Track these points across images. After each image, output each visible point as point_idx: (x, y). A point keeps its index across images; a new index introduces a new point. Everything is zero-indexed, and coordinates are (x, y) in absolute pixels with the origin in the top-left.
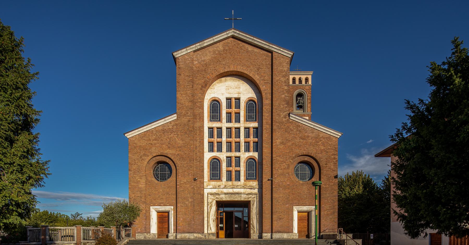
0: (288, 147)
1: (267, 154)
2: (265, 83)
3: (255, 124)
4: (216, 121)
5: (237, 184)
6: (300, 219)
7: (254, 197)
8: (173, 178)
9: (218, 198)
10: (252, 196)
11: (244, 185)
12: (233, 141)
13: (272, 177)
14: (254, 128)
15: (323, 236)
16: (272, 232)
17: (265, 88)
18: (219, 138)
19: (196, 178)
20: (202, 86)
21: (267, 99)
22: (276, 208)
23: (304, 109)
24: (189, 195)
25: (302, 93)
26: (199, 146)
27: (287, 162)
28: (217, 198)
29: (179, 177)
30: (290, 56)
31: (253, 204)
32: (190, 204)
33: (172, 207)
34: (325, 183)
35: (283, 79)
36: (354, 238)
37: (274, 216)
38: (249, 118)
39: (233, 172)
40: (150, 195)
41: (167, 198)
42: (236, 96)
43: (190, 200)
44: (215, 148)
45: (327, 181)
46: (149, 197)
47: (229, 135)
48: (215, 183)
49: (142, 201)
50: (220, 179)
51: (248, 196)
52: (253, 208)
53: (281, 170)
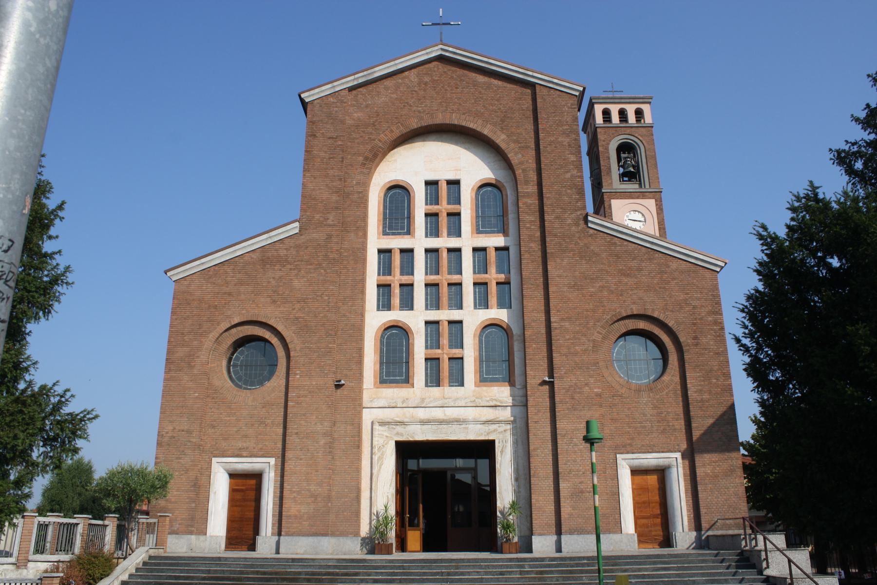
0: (591, 296)
1: (536, 315)
2: (520, 147)
3: (499, 241)
4: (399, 234)
6: (638, 491)
7: (505, 431)
8: (277, 382)
9: (402, 435)
10: (499, 427)
12: (444, 281)
13: (551, 375)
14: (497, 249)
15: (710, 538)
16: (559, 533)
17: (523, 159)
18: (408, 274)
19: (340, 381)
20: (366, 158)
21: (527, 182)
22: (568, 461)
23: (640, 181)
24: (319, 427)
25: (632, 143)
28: (398, 434)
29: (295, 379)
30: (577, 94)
31: (503, 448)
33: (272, 461)
34: (700, 388)
35: (566, 141)
36: (792, 544)
37: (563, 485)
38: (481, 228)
39: (443, 362)
40: (213, 427)
41: (260, 434)
42: (452, 177)
44: (396, 301)
45: (703, 383)
46: (211, 431)
47: (433, 267)
49: (190, 441)
50: (407, 380)
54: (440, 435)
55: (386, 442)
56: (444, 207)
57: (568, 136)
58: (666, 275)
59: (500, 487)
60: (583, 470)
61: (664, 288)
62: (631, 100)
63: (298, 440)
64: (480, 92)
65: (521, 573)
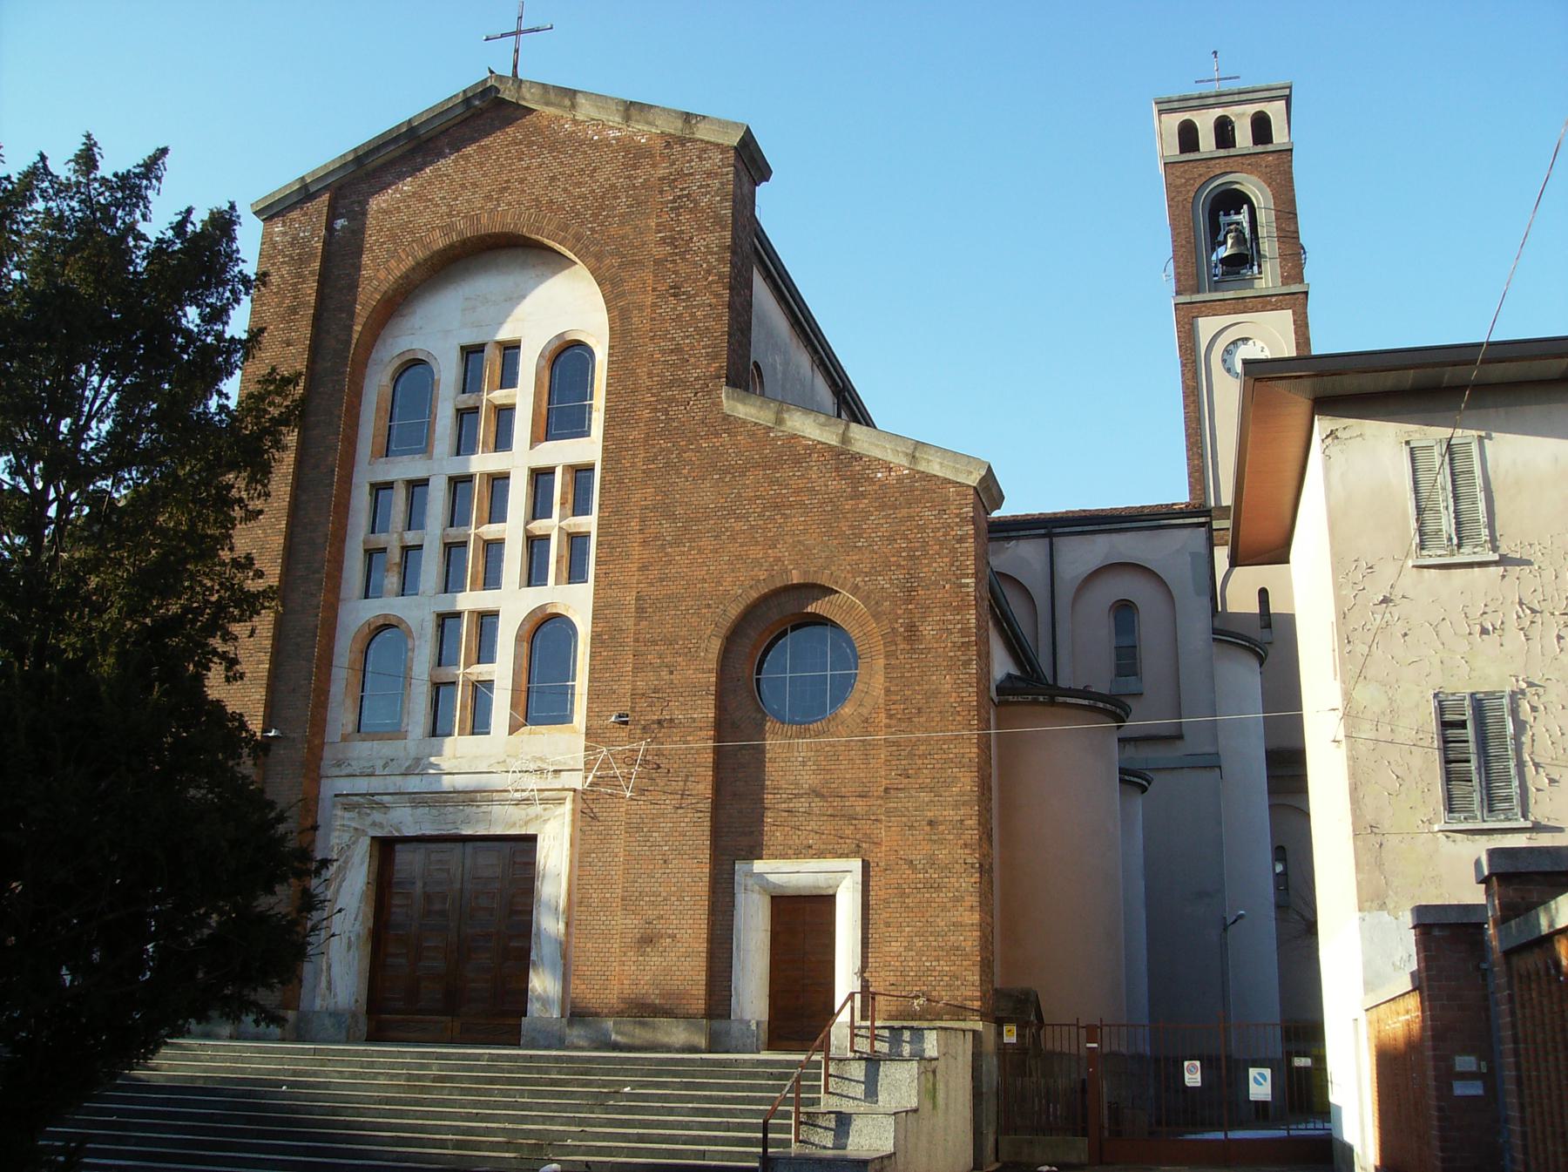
9: (381, 826)
10: (545, 809)
28: (374, 824)
48: (371, 749)
58: (867, 501)
60: (665, 894)
62: (1202, 102)
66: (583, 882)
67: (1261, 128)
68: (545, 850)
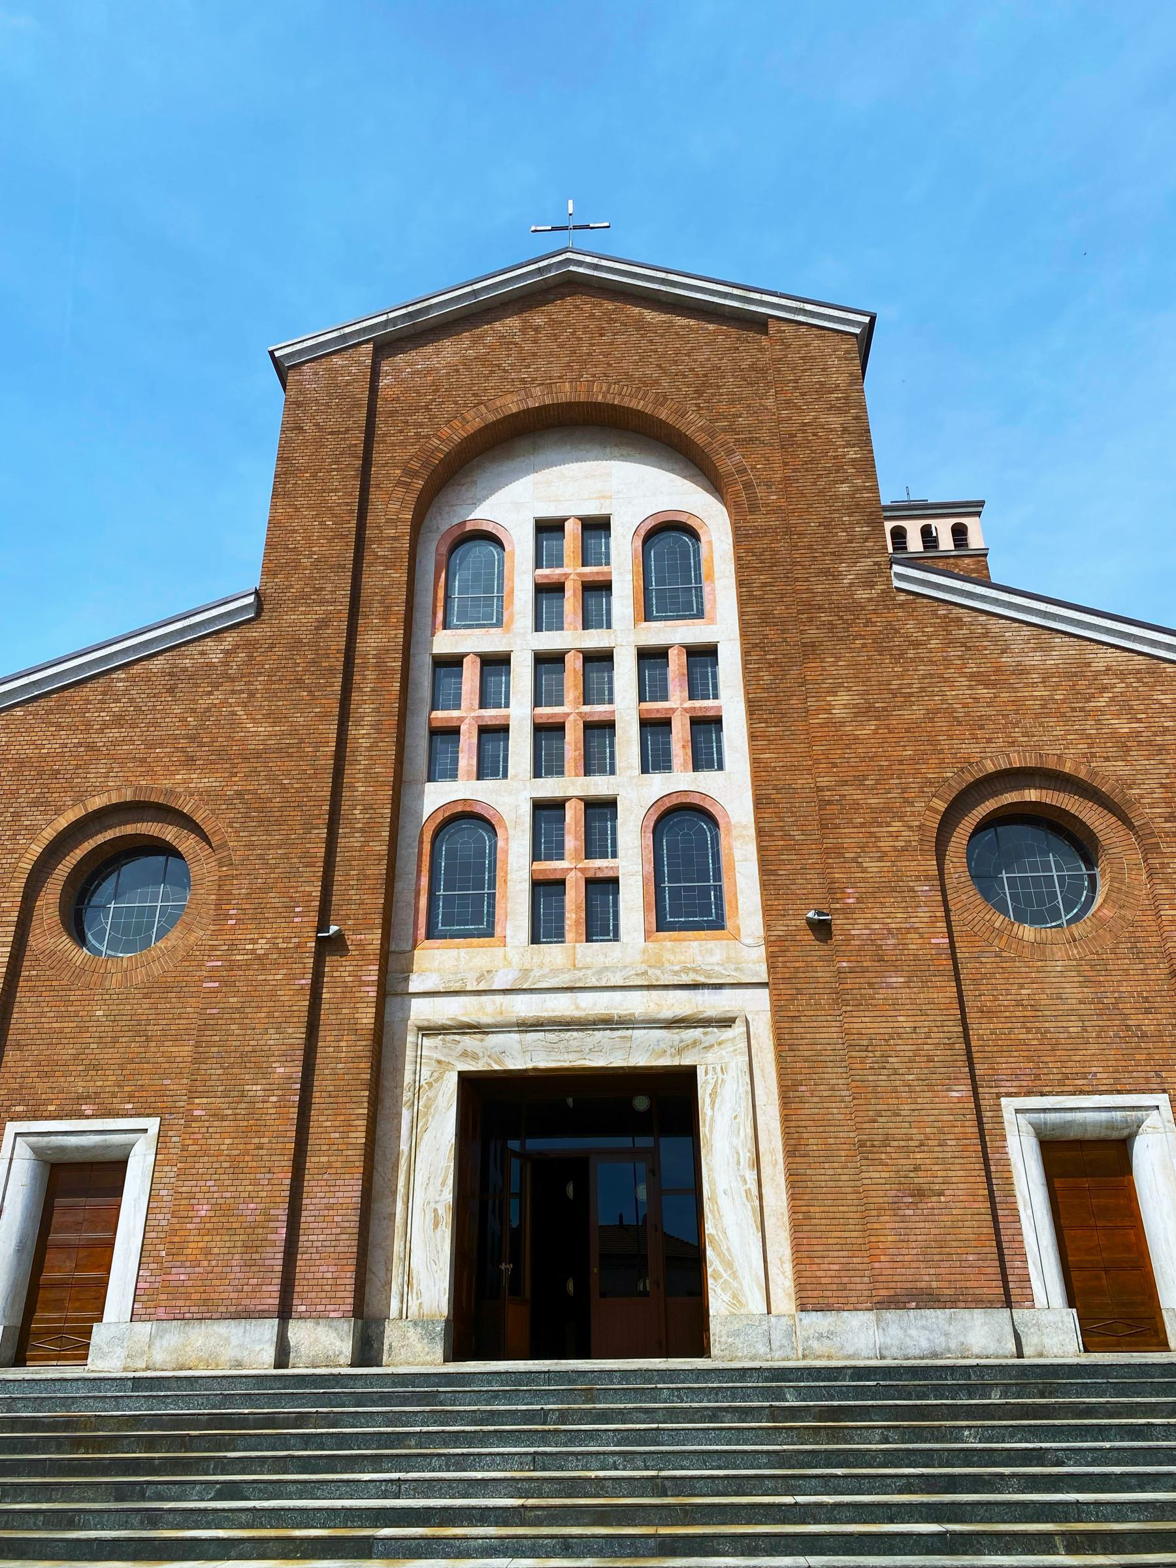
2: (737, 440)
5: (601, 958)
9: (475, 1057)
10: (705, 1034)
11: (644, 967)
26: (369, 749)
27: (913, 814)
28: (465, 1054)
30: (857, 331)
32: (274, 1099)
42: (592, 509)
43: (282, 1070)
48: (458, 959)
51: (676, 1037)
52: (712, 1117)
53: (880, 859)
54: (566, 1056)
55: (436, 1074)
56: (572, 571)
57: (840, 411)
59: (712, 1183)
61: (1082, 709)
63: (220, 1072)
64: (651, 341)
65: (774, 1414)
66: (792, 1124)
67: (959, 533)
68: (710, 1087)
